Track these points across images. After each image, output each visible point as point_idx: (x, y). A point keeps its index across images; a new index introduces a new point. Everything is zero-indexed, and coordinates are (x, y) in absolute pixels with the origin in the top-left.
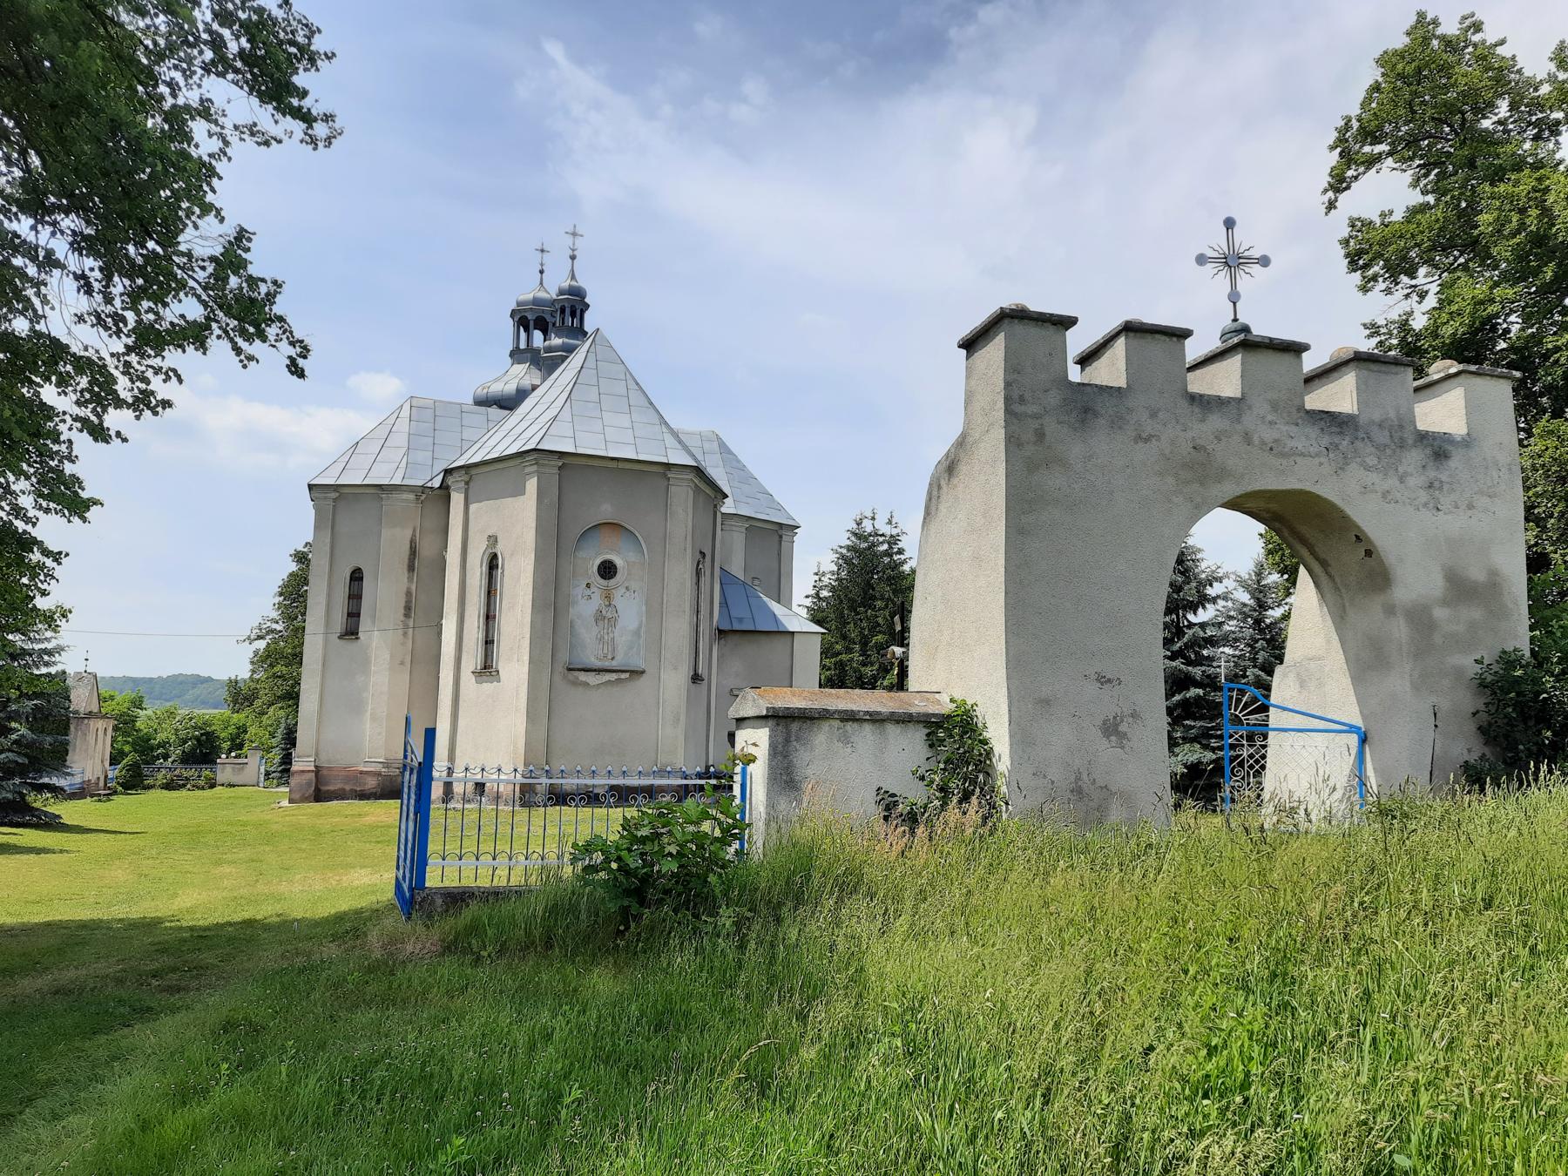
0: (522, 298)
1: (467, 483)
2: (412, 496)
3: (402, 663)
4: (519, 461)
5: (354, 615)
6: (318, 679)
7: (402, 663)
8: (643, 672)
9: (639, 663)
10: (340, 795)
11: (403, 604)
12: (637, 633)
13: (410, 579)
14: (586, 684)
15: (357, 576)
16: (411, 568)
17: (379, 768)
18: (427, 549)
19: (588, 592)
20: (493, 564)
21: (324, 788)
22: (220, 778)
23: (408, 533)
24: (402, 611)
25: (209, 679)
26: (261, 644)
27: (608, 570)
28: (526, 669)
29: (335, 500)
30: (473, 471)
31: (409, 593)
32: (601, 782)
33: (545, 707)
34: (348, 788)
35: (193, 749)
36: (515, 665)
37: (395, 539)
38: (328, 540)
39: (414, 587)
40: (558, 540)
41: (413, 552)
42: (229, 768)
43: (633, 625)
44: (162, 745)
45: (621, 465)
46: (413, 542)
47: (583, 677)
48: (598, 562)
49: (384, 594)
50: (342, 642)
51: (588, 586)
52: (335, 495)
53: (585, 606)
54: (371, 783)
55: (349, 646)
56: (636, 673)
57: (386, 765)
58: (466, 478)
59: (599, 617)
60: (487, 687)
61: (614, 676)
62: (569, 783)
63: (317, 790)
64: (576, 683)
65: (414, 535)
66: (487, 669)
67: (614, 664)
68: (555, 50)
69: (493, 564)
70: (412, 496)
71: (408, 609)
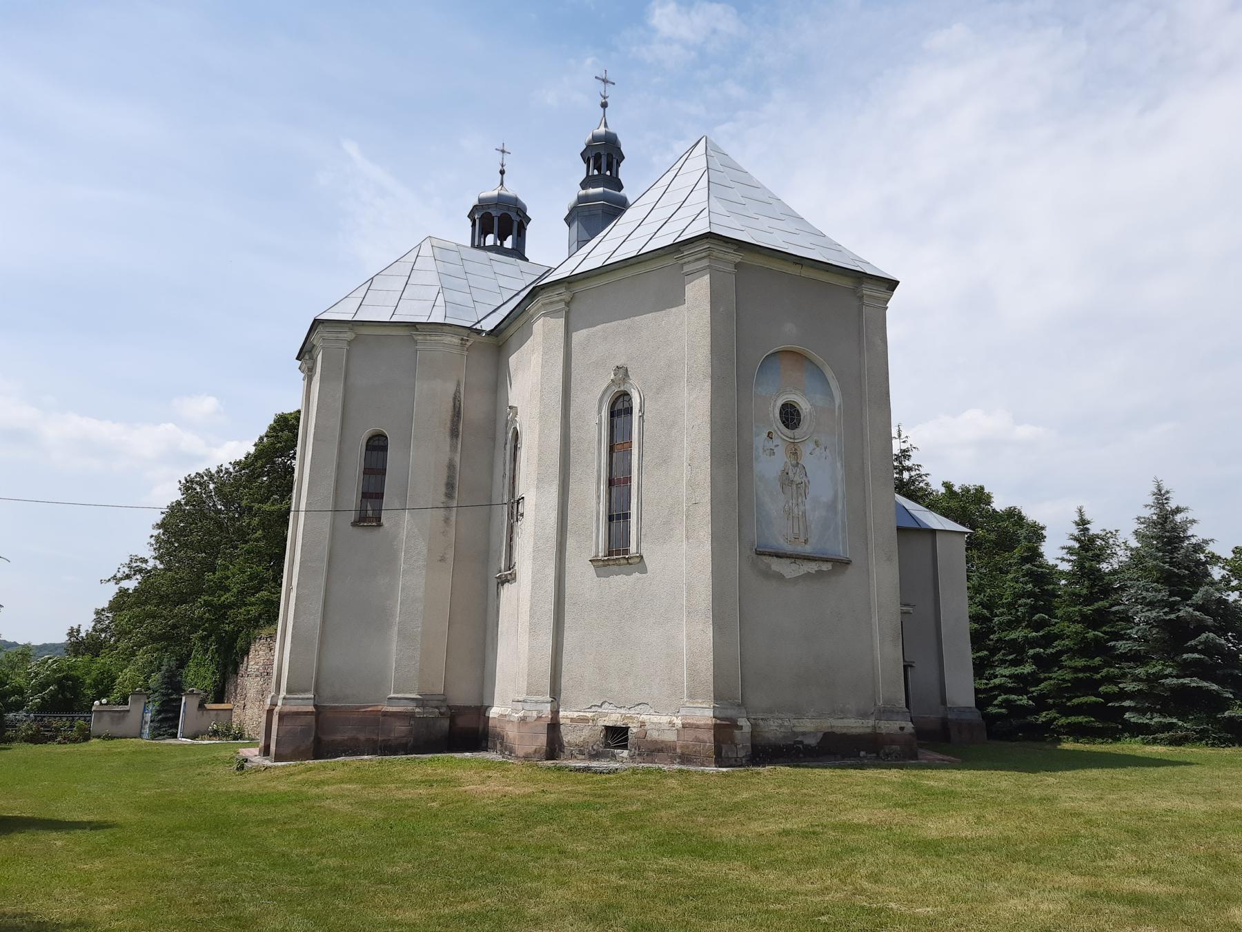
0: (483, 195)
1: (568, 304)
2: (456, 340)
3: (443, 560)
4: (669, 261)
5: (372, 494)
6: (322, 581)
7: (443, 560)
8: (848, 563)
9: (839, 549)
10: (353, 749)
11: (443, 479)
12: (832, 507)
13: (453, 448)
14: (780, 577)
15: (377, 445)
16: (454, 433)
17: (410, 707)
18: (475, 408)
19: (770, 444)
20: (620, 408)
21: (327, 738)
22: (94, 726)
23: (451, 388)
24: (443, 489)
25: (15, 644)
26: (131, 585)
27: (790, 416)
28: (707, 547)
29: (350, 343)
30: (578, 288)
31: (451, 466)
32: (809, 726)
33: (734, 609)
34: (362, 737)
35: (53, 695)
36: (681, 553)
37: (432, 394)
38: (340, 395)
39: (457, 459)
40: (741, 364)
41: (457, 413)
42: (106, 718)
43: (826, 497)
44: (19, 691)
45: (806, 273)
46: (456, 399)
47: (776, 565)
48: (780, 403)
49: (418, 463)
50: (358, 532)
51: (770, 435)
52: (349, 336)
53: (770, 464)
54: (400, 730)
55: (365, 536)
56: (841, 564)
57: (420, 702)
58: (566, 296)
59: (786, 481)
60: (621, 582)
61: (812, 567)
62: (774, 729)
63: (318, 741)
64: (768, 575)
65: (458, 391)
66: (618, 553)
67: (808, 549)
68: (351, 148)
69: (620, 408)
70: (456, 340)
71: (450, 486)
